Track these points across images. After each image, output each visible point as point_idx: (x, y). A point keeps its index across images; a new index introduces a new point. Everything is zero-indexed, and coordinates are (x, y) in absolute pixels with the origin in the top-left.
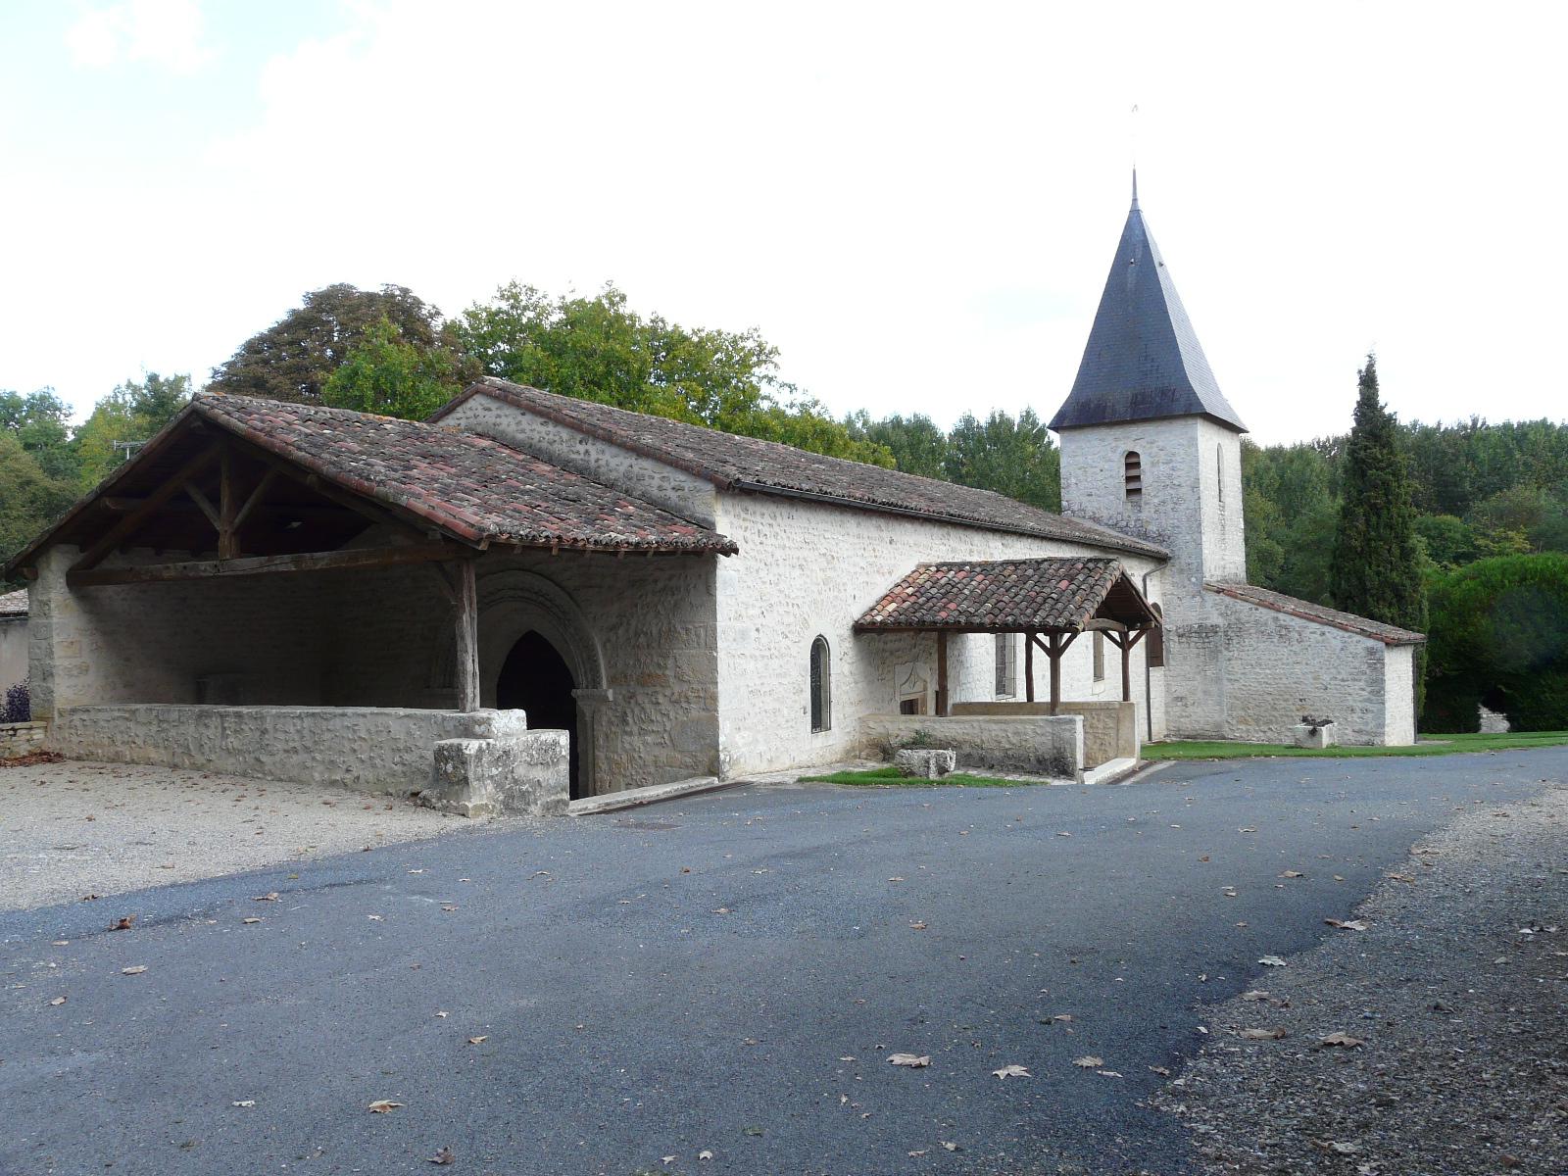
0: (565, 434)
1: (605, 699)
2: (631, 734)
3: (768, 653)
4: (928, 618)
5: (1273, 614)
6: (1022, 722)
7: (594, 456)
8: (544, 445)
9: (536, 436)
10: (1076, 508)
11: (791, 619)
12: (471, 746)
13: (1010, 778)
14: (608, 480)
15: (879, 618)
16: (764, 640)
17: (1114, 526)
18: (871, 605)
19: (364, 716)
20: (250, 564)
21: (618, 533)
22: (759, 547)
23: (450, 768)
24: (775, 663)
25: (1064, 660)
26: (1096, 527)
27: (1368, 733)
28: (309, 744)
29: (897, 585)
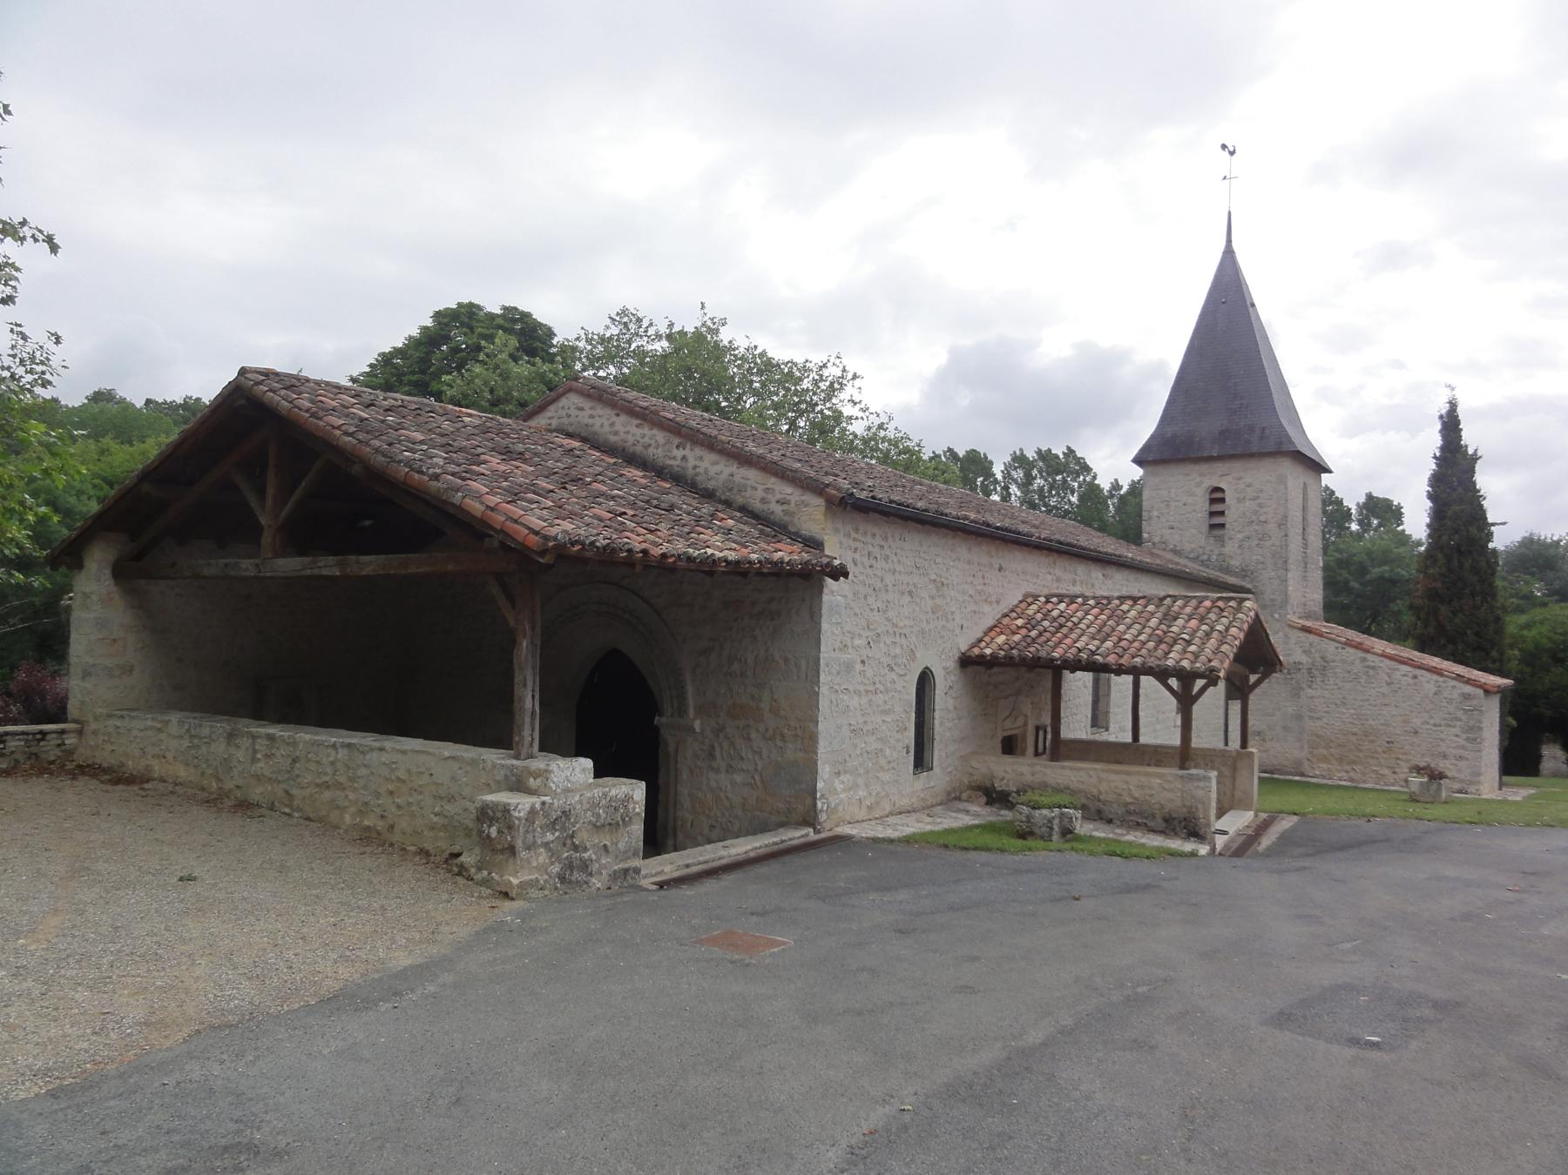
0: (660, 436)
1: (691, 730)
2: (717, 771)
3: (871, 688)
4: (1043, 654)
5: (1361, 654)
6: (1147, 775)
7: (692, 462)
8: (639, 449)
9: (631, 439)
10: (1156, 540)
11: (898, 651)
12: (522, 804)
13: (1130, 838)
14: (706, 489)
15: (988, 651)
16: (869, 673)
17: (1195, 559)
18: (980, 635)
19: (404, 752)
20: (289, 565)
21: (718, 546)
22: (869, 571)
23: (493, 832)
24: (880, 698)
25: (1197, 709)
26: (1177, 559)
27: (1461, 781)
28: (342, 779)
29: (1006, 615)
